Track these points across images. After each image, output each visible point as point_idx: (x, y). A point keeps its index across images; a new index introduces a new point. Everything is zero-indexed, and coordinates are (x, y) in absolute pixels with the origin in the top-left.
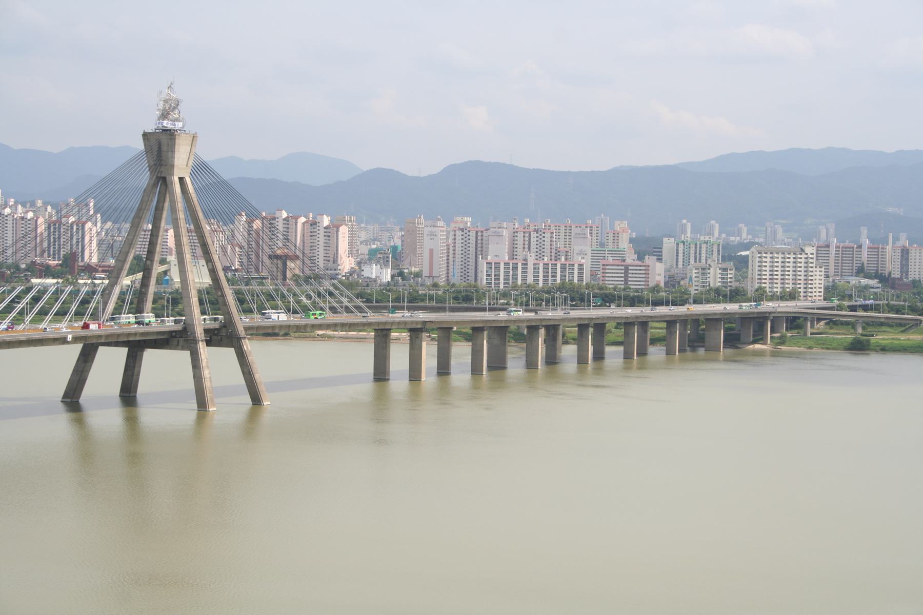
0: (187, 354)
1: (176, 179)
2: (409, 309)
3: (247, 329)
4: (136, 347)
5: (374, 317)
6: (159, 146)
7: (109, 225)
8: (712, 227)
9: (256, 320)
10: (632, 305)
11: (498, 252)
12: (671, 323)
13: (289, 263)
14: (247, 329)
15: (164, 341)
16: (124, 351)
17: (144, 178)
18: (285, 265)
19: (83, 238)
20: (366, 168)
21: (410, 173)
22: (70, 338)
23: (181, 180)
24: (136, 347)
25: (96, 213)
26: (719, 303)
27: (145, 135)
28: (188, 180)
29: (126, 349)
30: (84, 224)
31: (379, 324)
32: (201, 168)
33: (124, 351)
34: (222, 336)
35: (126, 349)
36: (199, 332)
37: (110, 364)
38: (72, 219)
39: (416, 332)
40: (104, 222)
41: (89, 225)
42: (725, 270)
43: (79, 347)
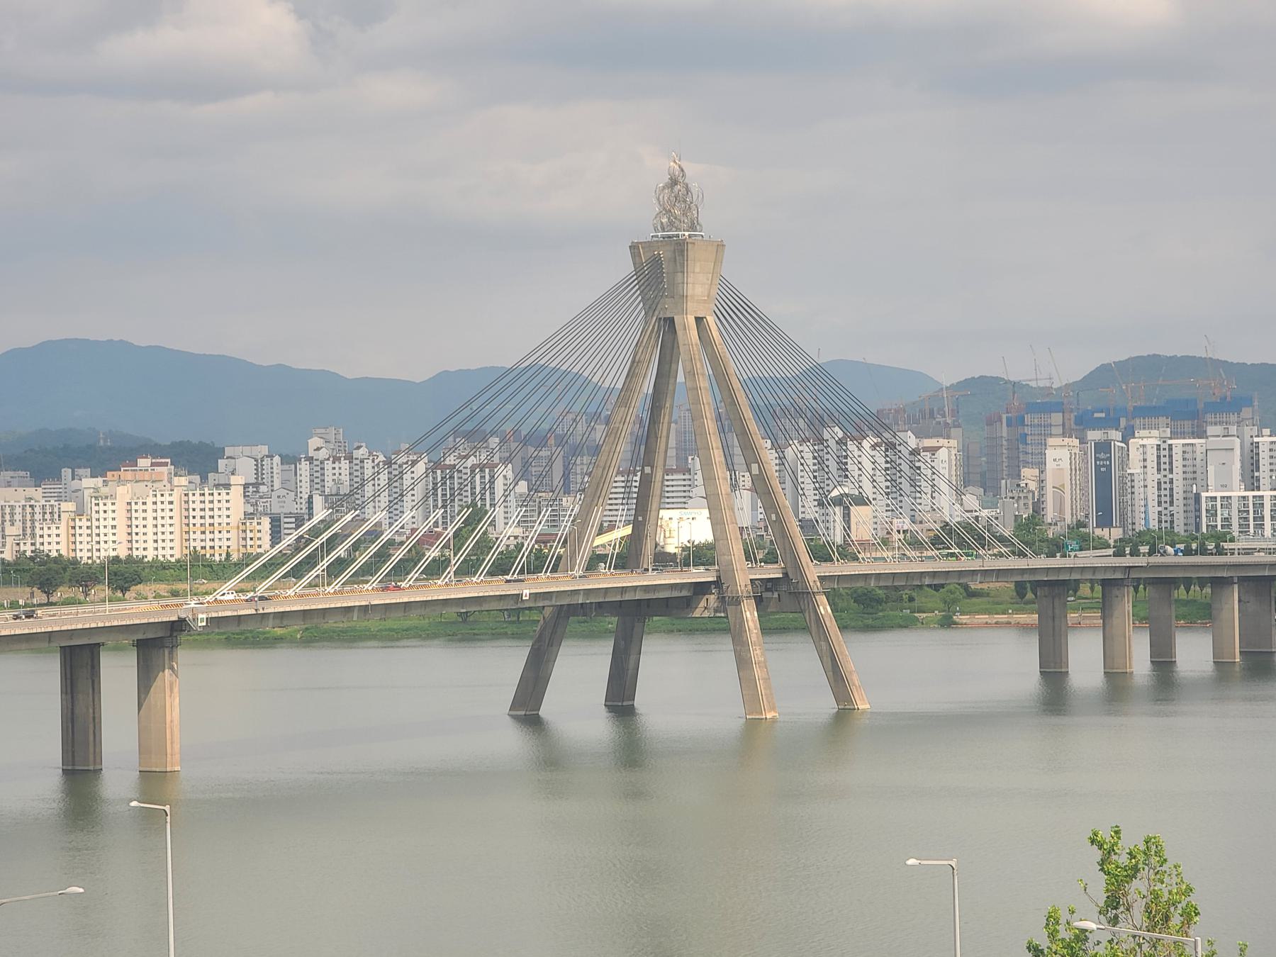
13: (854, 510)
18: (847, 516)
27: (634, 248)
28: (711, 320)
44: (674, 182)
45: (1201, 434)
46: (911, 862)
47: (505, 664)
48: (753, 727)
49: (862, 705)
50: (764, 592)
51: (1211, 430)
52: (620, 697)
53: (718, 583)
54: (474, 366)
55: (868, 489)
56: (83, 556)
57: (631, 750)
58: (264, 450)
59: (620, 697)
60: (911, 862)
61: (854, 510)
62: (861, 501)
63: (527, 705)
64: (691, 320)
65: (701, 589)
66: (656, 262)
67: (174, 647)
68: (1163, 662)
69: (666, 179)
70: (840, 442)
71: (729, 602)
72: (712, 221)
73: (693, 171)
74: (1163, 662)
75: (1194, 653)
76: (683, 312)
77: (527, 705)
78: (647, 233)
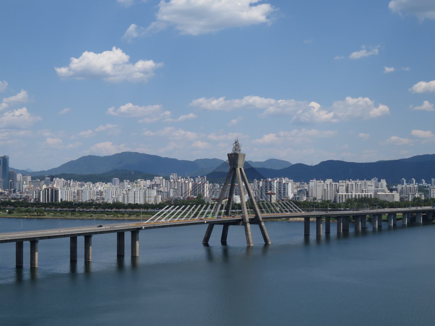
0: (40, 241)
1: (239, 169)
2: (316, 210)
3: (263, 218)
4: (226, 225)
5: (303, 213)
6: (233, 158)
7: (211, 184)
8: (413, 181)
9: (266, 215)
10: (391, 208)
11: (171, 195)
12: (404, 213)
13: (272, 196)
14: (263, 218)
15: (236, 223)
16: (222, 226)
17: (227, 169)
18: (271, 197)
19: (204, 190)
20: (294, 163)
21: (309, 164)
22: (205, 222)
23: (240, 169)
24: (226, 225)
25: (207, 180)
26: (414, 206)
27: (228, 155)
28: (243, 169)
29: (223, 226)
30: (204, 184)
31: (306, 216)
32: (246, 164)
33: (222, 226)
34: (255, 221)
35: (223, 226)
36: (247, 219)
37: (218, 230)
38: (200, 183)
39: (319, 218)
40: (209, 183)
41: (205, 184)
42: (421, 195)
43: (208, 225)
44: (236, 142)
45: (338, 182)
48: (249, 247)
49: (270, 243)
50: (252, 221)
51: (340, 181)
54: (203, 158)
55: (275, 192)
56: (126, 203)
57: (226, 251)
58: (162, 178)
62: (274, 194)
64: (239, 169)
67: (138, 232)
69: (235, 142)
71: (245, 224)
72: (243, 150)
76: (237, 167)
78: (230, 152)
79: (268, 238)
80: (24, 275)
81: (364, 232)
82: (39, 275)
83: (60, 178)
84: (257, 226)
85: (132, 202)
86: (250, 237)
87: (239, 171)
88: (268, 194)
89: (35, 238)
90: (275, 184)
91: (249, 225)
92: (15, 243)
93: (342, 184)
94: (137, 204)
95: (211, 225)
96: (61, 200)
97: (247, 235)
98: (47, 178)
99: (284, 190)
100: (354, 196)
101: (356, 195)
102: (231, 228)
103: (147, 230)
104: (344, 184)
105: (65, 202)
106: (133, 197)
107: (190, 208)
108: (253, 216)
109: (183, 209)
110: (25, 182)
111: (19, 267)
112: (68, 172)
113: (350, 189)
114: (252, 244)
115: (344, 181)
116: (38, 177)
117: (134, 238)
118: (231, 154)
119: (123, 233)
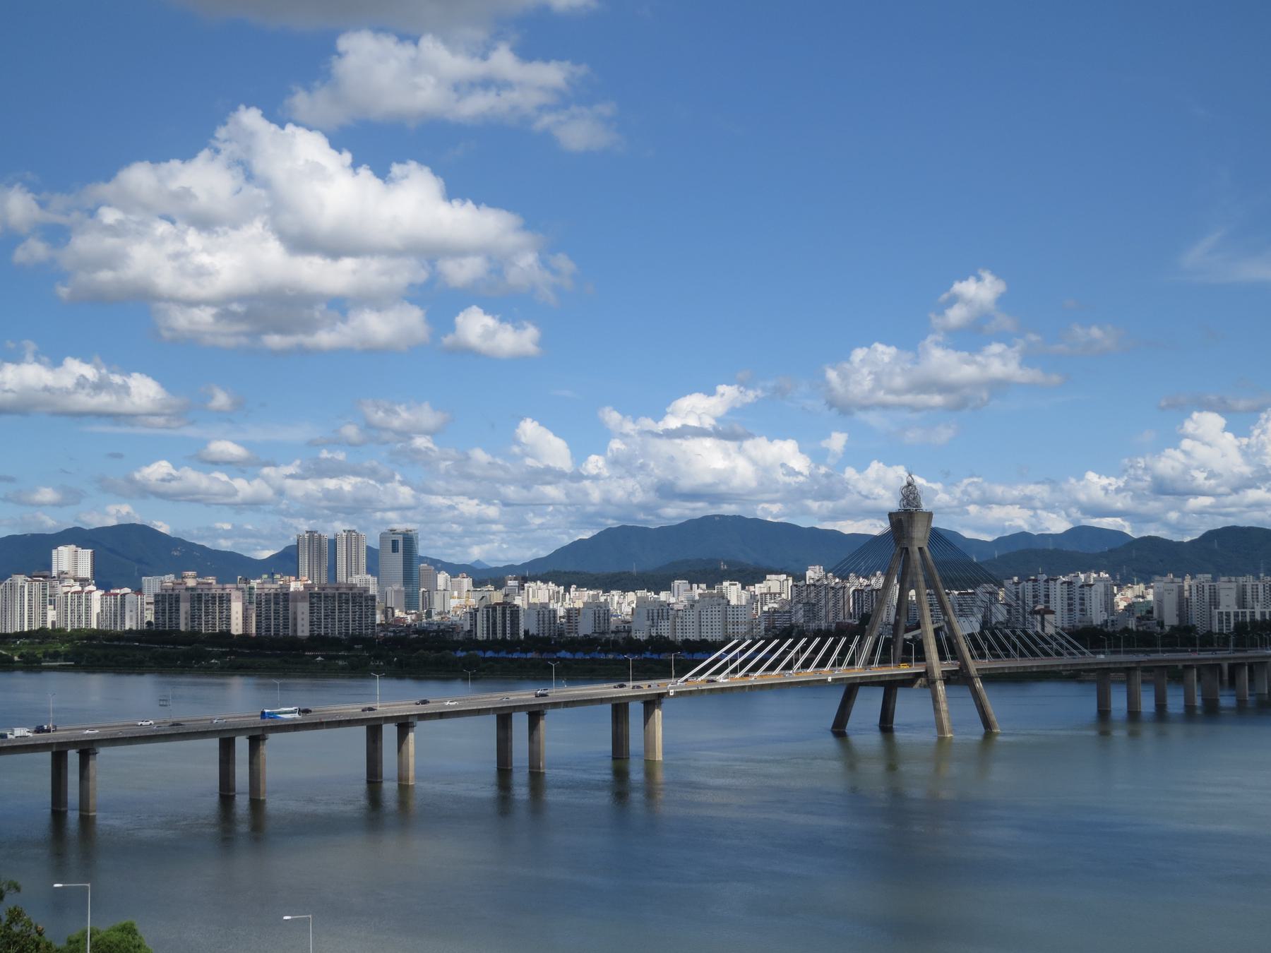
4: (890, 687)
9: (987, 664)
13: (1047, 617)
18: (1043, 619)
22: (830, 679)
23: (920, 549)
27: (890, 514)
28: (926, 549)
34: (957, 679)
36: (973, 671)
46: (286, 918)
47: (833, 702)
50: (949, 679)
52: (886, 724)
53: (926, 673)
59: (886, 724)
60: (286, 918)
61: (1047, 617)
63: (839, 729)
65: (918, 675)
66: (900, 521)
68: (1161, 706)
70: (1047, 581)
71: (931, 683)
73: (919, 481)
74: (1161, 706)
75: (1175, 702)
77: (839, 729)
79: (993, 717)
80: (69, 833)
81: (1211, 711)
82: (415, 803)
83: (545, 581)
84: (966, 692)
85: (693, 636)
86: (944, 715)
87: (917, 555)
88: (1038, 612)
89: (408, 716)
90: (1057, 591)
91: (941, 687)
92: (364, 728)
93: (1229, 585)
94: (705, 641)
95: (851, 689)
96: (526, 632)
97: (937, 710)
98: (511, 583)
99: (1082, 604)
100: (1258, 617)
101: (1263, 614)
102: (902, 696)
103: (681, 699)
104: (1233, 585)
105: (60, 630)
106: (696, 624)
107: (792, 646)
108: (951, 665)
109: (803, 650)
110: (456, 594)
111: (58, 813)
112: (570, 567)
113: (1249, 597)
114: (951, 732)
115: (1233, 579)
116: (483, 576)
117: (256, 742)
118: (896, 514)
119: (626, 705)
